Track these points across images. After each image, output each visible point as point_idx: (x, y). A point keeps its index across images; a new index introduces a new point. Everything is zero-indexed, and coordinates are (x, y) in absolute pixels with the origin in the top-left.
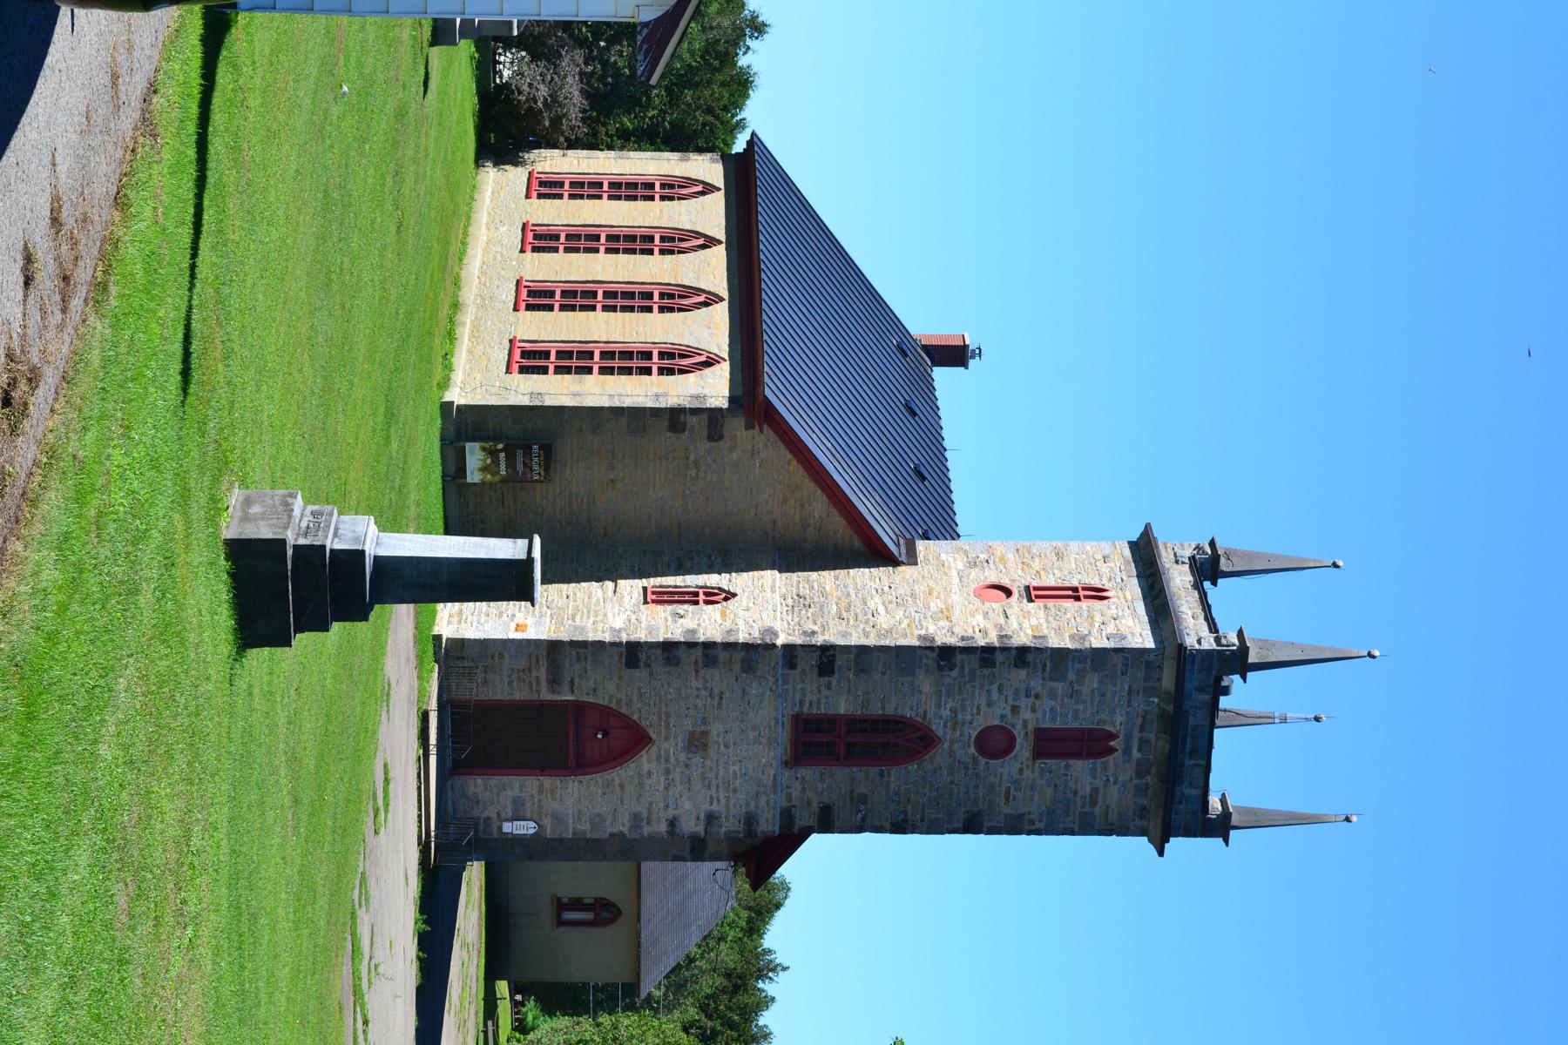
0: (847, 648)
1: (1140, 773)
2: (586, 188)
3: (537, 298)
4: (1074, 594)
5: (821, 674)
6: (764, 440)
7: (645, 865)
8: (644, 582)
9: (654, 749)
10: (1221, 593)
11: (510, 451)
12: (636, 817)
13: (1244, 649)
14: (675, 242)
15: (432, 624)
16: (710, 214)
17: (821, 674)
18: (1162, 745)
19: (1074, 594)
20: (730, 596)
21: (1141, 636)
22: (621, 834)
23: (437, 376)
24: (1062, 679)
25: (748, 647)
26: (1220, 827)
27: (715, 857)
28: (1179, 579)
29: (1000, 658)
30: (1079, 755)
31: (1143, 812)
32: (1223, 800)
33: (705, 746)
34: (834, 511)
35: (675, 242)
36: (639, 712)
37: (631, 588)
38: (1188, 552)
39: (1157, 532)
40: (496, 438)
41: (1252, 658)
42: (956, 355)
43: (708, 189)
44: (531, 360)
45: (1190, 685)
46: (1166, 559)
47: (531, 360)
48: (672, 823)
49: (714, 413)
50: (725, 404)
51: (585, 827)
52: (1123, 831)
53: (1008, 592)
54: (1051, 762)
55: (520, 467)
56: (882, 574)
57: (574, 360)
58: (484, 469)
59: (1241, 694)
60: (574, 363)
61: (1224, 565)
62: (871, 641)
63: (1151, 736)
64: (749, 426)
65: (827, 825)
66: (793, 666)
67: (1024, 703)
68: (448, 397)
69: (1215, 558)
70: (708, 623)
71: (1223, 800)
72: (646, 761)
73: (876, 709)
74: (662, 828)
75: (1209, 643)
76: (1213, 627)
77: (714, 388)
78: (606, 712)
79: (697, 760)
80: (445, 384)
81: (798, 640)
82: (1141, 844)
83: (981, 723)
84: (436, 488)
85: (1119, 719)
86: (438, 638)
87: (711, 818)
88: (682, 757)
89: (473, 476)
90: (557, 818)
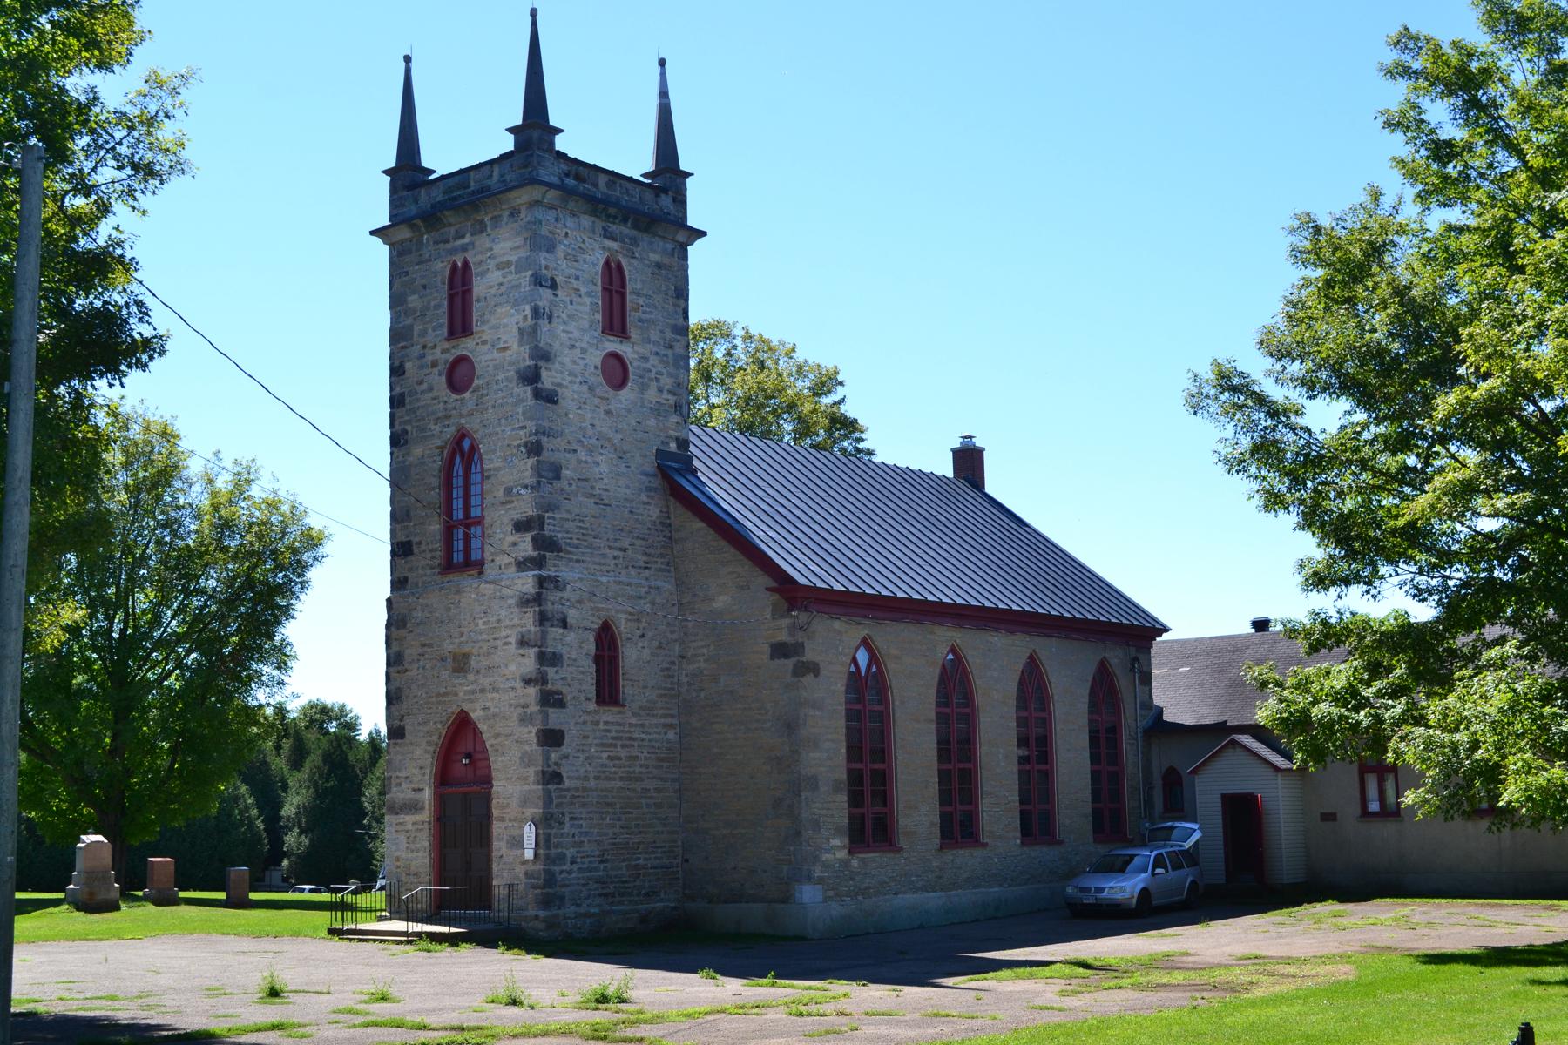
88: (471, 677)
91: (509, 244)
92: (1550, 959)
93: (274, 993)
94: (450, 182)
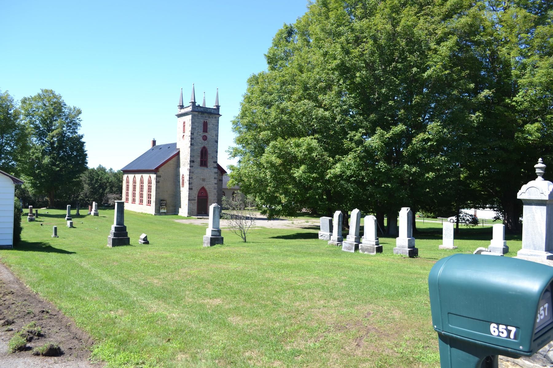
0: (190, 158)
1: (210, 118)
2: (127, 195)
3: (141, 201)
4: (184, 126)
5: (194, 162)
6: (160, 169)
7: (223, 188)
8: (181, 187)
9: (205, 186)
10: (185, 105)
11: (161, 206)
12: (214, 189)
13: (192, 102)
14: (142, 182)
15: (185, 217)
16: (131, 176)
17: (194, 162)
18: (206, 114)
19: (184, 126)
20: (183, 175)
21: (190, 117)
22: (217, 191)
23: (151, 216)
24: (196, 128)
25: (190, 172)
26: (218, 107)
27: (222, 178)
28: (183, 111)
29: (192, 137)
30: (207, 126)
31: (215, 118)
32: (214, 106)
33: (204, 179)
34: (172, 160)
35: (142, 182)
36: (199, 188)
37: (182, 189)
38: (179, 110)
39: (176, 114)
40: (160, 208)
41: (193, 101)
42: (154, 142)
43: (128, 177)
44: (149, 202)
45: (197, 110)
46: (180, 113)
47: (149, 202)
48: (215, 184)
49: (157, 177)
50: (155, 175)
51: (216, 196)
52: (218, 120)
53: (184, 135)
54: (208, 130)
55: (164, 204)
56: (181, 153)
57: (149, 196)
58: (164, 209)
59: (199, 103)
60: (150, 196)
61: (181, 105)
62: (189, 155)
63: (204, 116)
64: (159, 172)
65: (216, 162)
66: (193, 166)
67: (199, 134)
68: (154, 215)
69: (180, 106)
70: (187, 178)
71: (214, 106)
72: (206, 187)
73: (200, 155)
74: (216, 185)
75: (191, 107)
76: (189, 106)
77: (153, 176)
78: (199, 193)
79: (206, 180)
80: (152, 215)
81: (189, 165)
82: (220, 118)
83: (202, 140)
84: (166, 216)
85: (202, 120)
86: (187, 216)
87: (215, 178)
88: (206, 182)
89: (165, 211)
90: (214, 200)
91: (215, 122)
92: (516, 236)
93: (42, 225)
94: (205, 109)
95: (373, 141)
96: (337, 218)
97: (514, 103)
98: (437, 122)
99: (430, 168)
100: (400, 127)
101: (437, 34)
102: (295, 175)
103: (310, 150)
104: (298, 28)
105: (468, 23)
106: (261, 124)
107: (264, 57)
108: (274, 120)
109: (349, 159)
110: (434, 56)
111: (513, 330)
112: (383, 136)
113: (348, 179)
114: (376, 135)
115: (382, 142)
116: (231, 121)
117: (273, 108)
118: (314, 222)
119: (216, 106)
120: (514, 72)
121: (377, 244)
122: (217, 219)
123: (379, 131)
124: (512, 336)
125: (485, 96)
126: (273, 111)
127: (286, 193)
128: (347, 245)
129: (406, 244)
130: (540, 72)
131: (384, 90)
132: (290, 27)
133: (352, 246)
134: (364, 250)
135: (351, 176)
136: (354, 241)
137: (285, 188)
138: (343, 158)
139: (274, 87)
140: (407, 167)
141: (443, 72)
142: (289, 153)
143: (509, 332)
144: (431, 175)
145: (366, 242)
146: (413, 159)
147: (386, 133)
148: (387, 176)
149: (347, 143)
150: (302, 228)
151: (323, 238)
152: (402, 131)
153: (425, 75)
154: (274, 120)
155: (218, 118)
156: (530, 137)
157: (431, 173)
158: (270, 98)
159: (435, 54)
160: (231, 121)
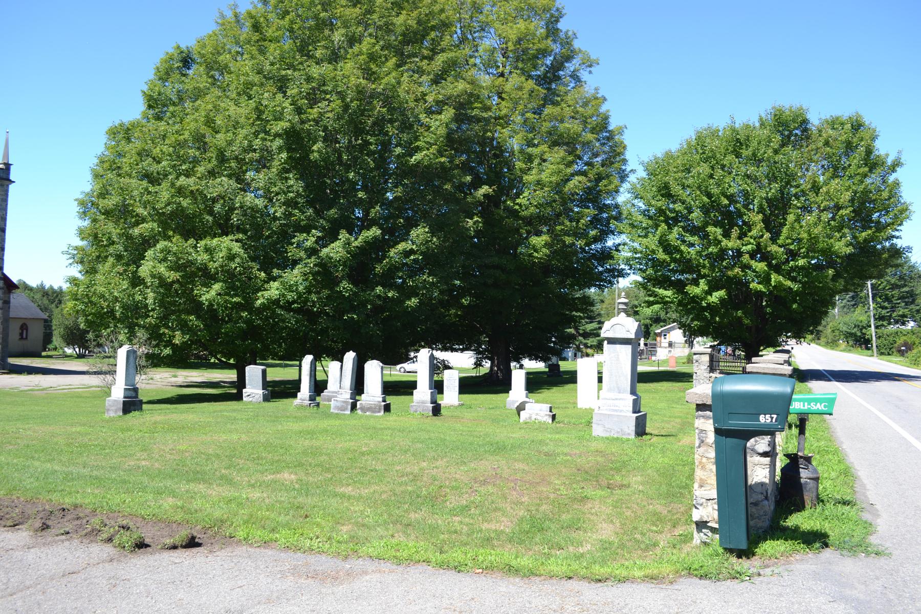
7: (11, 316)
26: (8, 166)
82: (11, 186)
95: (335, 250)
96: (309, 366)
97: (517, 207)
98: (424, 227)
99: (413, 292)
100: (375, 232)
101: (426, 102)
102: (203, 298)
103: (231, 257)
104: (203, 56)
105: (466, 92)
106: (141, 211)
107: (142, 94)
108: (166, 206)
109: (294, 276)
110: (426, 134)
111: (775, 416)
112: (349, 244)
113: (288, 307)
114: (338, 241)
115: (348, 252)
116: (76, 200)
117: (165, 185)
118: (188, 376)
119: (5, 164)
120: (519, 165)
121: (384, 401)
122: (132, 370)
123: (343, 235)
124: (774, 420)
125: (484, 195)
126: (164, 193)
127: (184, 327)
128: (339, 404)
129: (428, 397)
130: (549, 168)
131: (352, 174)
132: (186, 51)
133: (347, 405)
134: (364, 409)
135: (294, 302)
136: (349, 397)
137: (182, 320)
138: (285, 273)
139: (164, 150)
140: (380, 291)
141: (437, 158)
142: (191, 263)
143: (772, 418)
144: (413, 302)
145: (368, 399)
146: (387, 280)
147: (353, 239)
148: (349, 304)
149: (292, 252)
150: (177, 386)
151: (251, 399)
152: (375, 238)
153: (413, 160)
154: (166, 206)
155: (8, 186)
156: (536, 254)
157: (413, 300)
158: (154, 168)
159: (426, 131)
160: (76, 200)
